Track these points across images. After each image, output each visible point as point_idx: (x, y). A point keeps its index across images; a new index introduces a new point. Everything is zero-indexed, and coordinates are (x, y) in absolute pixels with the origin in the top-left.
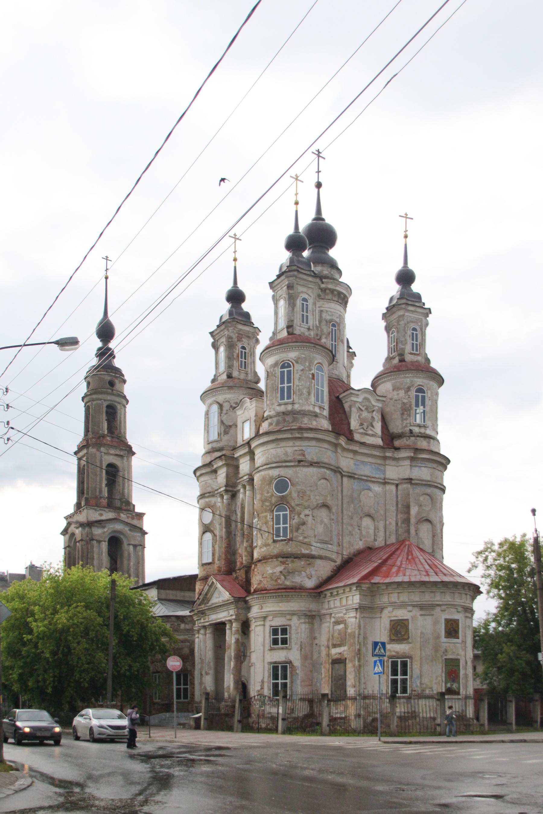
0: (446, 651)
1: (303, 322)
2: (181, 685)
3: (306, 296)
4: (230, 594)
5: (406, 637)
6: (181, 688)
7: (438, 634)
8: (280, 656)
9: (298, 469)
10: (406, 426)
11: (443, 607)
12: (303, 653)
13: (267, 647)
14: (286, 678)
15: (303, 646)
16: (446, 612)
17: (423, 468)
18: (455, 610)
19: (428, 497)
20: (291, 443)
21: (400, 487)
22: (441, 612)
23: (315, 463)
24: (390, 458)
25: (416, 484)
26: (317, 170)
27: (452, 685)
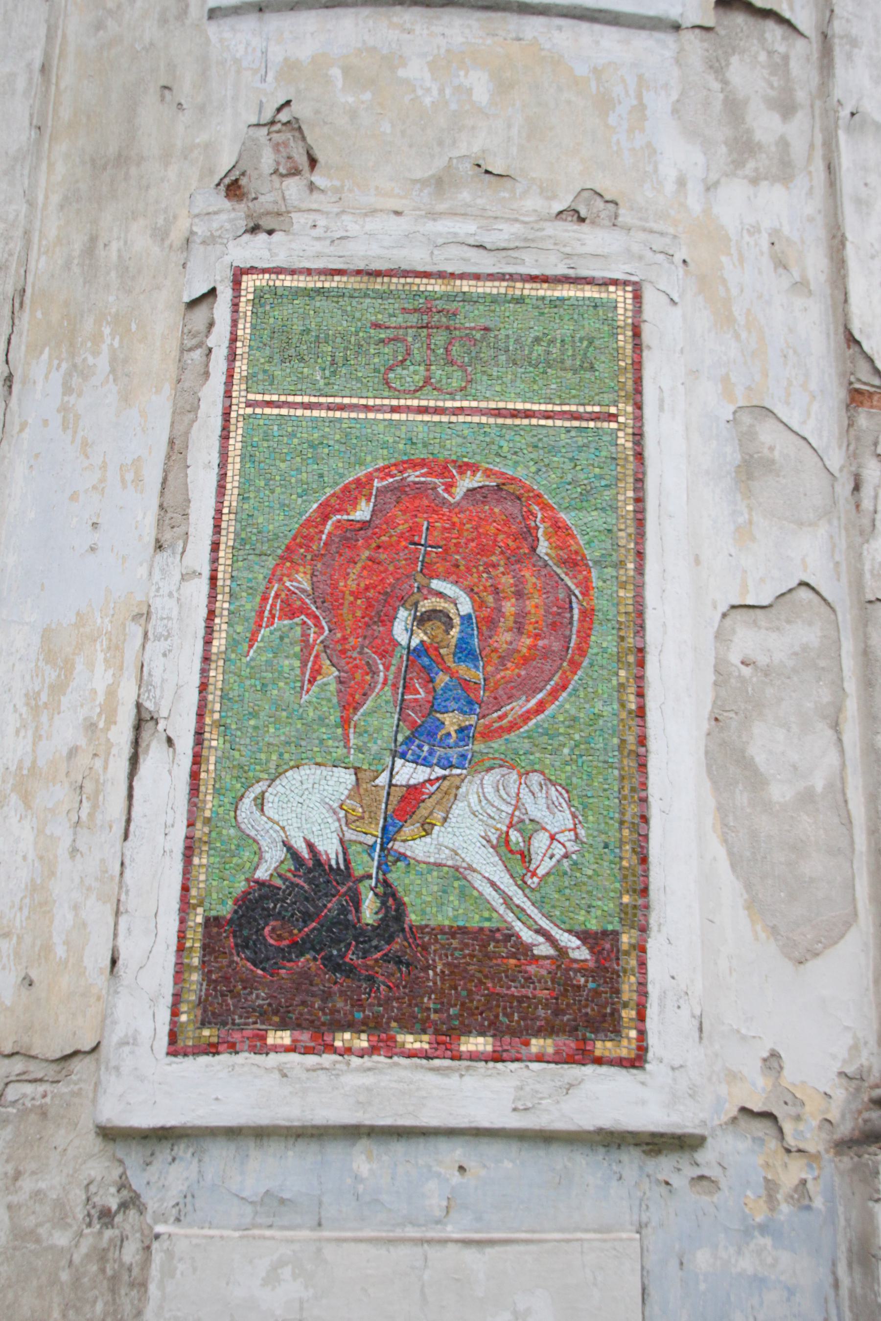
0: (293, 140)
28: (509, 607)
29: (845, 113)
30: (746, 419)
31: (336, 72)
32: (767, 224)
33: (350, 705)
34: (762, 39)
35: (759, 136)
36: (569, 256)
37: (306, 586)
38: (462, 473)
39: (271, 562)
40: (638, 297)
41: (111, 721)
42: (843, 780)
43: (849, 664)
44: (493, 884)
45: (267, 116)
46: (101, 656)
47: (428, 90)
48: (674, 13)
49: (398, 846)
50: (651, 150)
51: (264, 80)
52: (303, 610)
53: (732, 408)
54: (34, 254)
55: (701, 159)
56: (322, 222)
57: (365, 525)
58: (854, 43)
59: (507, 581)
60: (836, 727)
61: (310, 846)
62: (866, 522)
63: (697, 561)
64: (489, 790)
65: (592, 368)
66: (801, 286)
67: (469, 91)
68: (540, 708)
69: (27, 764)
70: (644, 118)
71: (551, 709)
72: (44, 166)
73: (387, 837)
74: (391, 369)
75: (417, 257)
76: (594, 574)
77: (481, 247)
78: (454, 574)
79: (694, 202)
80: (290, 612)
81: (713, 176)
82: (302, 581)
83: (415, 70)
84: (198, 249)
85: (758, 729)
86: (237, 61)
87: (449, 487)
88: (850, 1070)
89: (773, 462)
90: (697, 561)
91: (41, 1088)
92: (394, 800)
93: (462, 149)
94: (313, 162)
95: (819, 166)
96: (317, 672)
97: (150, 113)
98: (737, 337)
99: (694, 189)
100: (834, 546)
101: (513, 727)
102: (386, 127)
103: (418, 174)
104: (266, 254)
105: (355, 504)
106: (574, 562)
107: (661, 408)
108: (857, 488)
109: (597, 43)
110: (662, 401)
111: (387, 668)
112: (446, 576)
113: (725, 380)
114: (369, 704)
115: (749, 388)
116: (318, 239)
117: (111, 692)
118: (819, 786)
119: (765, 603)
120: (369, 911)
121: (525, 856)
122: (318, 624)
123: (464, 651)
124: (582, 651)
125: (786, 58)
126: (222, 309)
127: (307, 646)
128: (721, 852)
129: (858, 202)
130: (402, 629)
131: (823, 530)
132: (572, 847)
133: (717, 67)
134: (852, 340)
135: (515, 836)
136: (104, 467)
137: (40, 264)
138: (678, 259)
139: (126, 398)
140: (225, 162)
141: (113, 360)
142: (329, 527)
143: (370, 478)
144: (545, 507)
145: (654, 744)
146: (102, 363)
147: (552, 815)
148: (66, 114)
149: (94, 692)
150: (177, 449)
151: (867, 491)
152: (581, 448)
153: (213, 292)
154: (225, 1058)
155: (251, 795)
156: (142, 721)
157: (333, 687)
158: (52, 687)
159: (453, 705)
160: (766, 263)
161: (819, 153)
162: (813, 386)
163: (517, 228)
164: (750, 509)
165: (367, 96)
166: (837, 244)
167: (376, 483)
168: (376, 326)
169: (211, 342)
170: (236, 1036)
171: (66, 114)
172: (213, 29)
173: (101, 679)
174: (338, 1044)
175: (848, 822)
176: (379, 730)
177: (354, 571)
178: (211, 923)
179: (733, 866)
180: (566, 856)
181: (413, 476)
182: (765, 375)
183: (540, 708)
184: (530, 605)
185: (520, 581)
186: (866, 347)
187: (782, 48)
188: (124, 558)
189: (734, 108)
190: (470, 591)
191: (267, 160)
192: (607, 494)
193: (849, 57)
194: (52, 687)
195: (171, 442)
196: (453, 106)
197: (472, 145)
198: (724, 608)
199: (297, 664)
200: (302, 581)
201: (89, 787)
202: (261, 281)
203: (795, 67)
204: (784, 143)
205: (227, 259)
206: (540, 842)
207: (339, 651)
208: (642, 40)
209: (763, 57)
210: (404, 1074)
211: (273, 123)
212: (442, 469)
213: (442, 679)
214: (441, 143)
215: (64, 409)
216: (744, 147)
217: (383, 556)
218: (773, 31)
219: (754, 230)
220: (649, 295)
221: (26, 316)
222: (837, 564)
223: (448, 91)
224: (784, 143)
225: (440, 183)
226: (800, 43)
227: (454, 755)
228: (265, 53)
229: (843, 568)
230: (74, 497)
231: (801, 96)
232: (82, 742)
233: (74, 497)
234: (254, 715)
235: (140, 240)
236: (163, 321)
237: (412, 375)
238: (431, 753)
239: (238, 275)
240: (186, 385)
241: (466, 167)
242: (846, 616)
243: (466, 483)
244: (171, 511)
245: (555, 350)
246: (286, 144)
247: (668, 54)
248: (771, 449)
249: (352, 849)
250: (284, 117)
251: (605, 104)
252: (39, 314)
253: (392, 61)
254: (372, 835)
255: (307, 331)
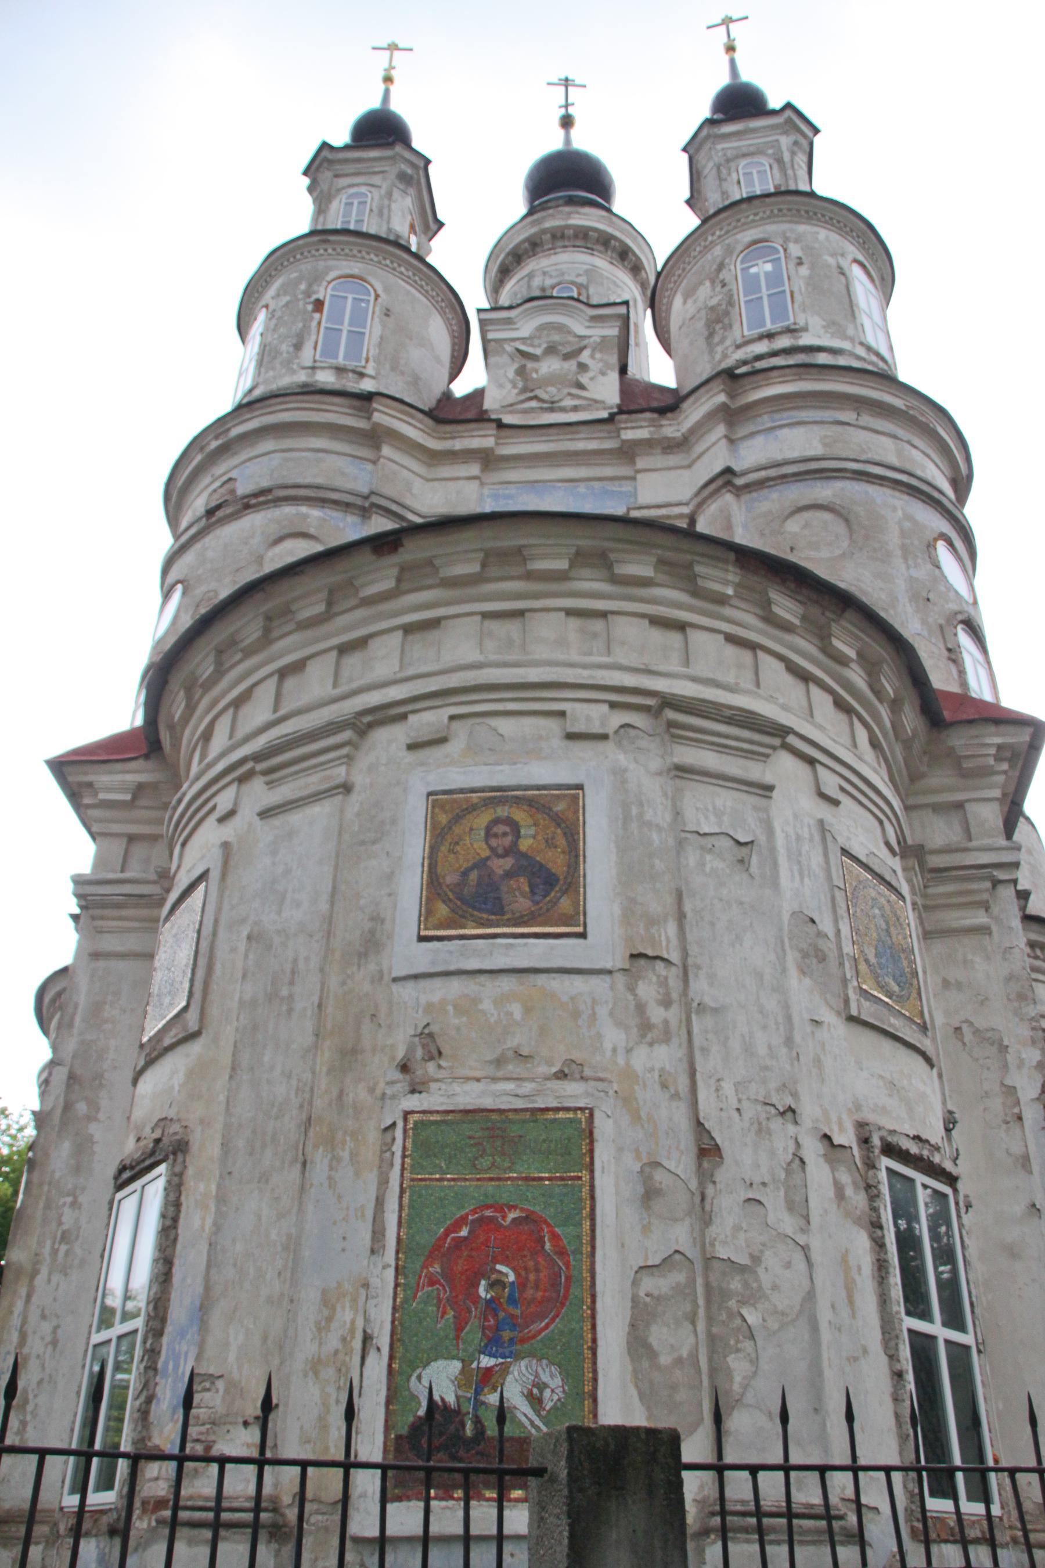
0: (430, 1045)
4: (40, 1118)
7: (377, 919)
10: (725, 356)
11: (427, 721)
16: (455, 747)
17: (785, 431)
18: (552, 725)
19: (827, 516)
22: (410, 757)
23: (256, 495)
24: (648, 445)
25: (761, 484)
26: (563, 103)
28: (532, 1277)
29: (695, 1005)
30: (647, 1169)
31: (450, 1008)
32: (657, 1066)
33: (459, 1329)
34: (654, 970)
35: (654, 1020)
36: (558, 1097)
37: (439, 1270)
38: (510, 1210)
39: (423, 1258)
40: (591, 1115)
41: (353, 1337)
42: (697, 1350)
43: (700, 1290)
44: (525, 1415)
45: (419, 1030)
46: (348, 1305)
47: (492, 1015)
48: (609, 965)
49: (482, 1398)
50: (599, 1036)
51: (417, 1012)
52: (438, 1282)
53: (640, 1165)
54: (315, 1098)
55: (623, 1036)
56: (443, 1087)
57: (465, 1238)
58: (699, 967)
59: (531, 1264)
60: (693, 1323)
61: (443, 1399)
62: (707, 1217)
63: (623, 1246)
64: (523, 1368)
65: (570, 1154)
66: (676, 1096)
67: (512, 1014)
68: (547, 1326)
69: (316, 1357)
70: (595, 1019)
71: (552, 1326)
72: (319, 1053)
73: (477, 1393)
74: (476, 1159)
75: (488, 1103)
76: (571, 1258)
77: (517, 1096)
78: (506, 1262)
79: (621, 1060)
80: (432, 1283)
81: (630, 1045)
82: (436, 1268)
83: (486, 1005)
84: (388, 1101)
85: (654, 1328)
86: (405, 1003)
87: (504, 1217)
88: (698, 1498)
89: (661, 1189)
90: (623, 1246)
91: (325, 1517)
92: (480, 1375)
93: (509, 1045)
94: (440, 1053)
95: (684, 1031)
96: (444, 1313)
97: (366, 1027)
98: (643, 1126)
99: (621, 1052)
100: (693, 1230)
101: (534, 1337)
102: (474, 1035)
103: (489, 1058)
104: (418, 1104)
105: (460, 1229)
106: (562, 1253)
107: (603, 1172)
108: (703, 1199)
109: (572, 984)
110: (603, 1168)
111: (476, 1309)
112: (502, 1263)
113: (637, 1150)
114: (468, 1328)
115: (648, 1153)
116: (442, 1095)
117: (353, 1322)
118: (685, 1355)
119: (657, 1263)
120: (469, 1430)
121: (540, 1401)
122: (446, 1291)
123: (512, 1300)
124: (566, 1297)
125: (666, 978)
126: (399, 1133)
127: (439, 1300)
128: (634, 1392)
129: (703, 1049)
130: (483, 1291)
131: (687, 1222)
132: (562, 1395)
133: (632, 989)
134: (699, 1124)
135: (535, 1391)
136: (348, 1208)
137: (318, 1103)
138: (611, 1093)
139: (357, 1174)
140: (400, 1054)
141: (351, 1153)
142: (449, 1240)
143: (467, 1215)
144: (549, 1225)
145: (601, 1342)
146: (346, 1155)
147: (554, 1381)
148: (329, 1026)
149: (345, 1322)
150: (380, 1202)
151: (708, 1201)
152: (565, 1195)
153: (394, 1124)
154: (405, 1504)
155: (415, 1375)
156: (367, 1338)
157: (451, 1320)
158: (327, 1319)
159: (507, 1327)
160: (657, 1087)
161: (684, 1023)
162: (682, 1147)
163: (533, 1085)
164: (649, 1216)
165: (464, 1019)
166: (692, 1073)
167: (470, 1217)
168: (470, 1137)
169: (394, 1149)
170: (410, 1493)
171: (329, 1026)
172: (395, 988)
173: (348, 1316)
174: (456, 1495)
175: (699, 1371)
176: (473, 1340)
177: (460, 1262)
178: (399, 1437)
179: (641, 1399)
180: (559, 1400)
181: (488, 1213)
182: (657, 1144)
183: (547, 1326)
184: (542, 1275)
185: (537, 1263)
186: (706, 1126)
187: (664, 973)
188: (357, 1256)
189: (641, 1008)
190: (514, 1269)
191: (419, 1053)
192: (577, 1218)
193: (696, 976)
194: (327, 1319)
195: (377, 1199)
196: (504, 1022)
197: (512, 1042)
198: (636, 1268)
199: (435, 1309)
200: (436, 1268)
201: (344, 1370)
202: (416, 1117)
203: (672, 982)
204: (666, 1022)
205: (401, 1107)
206: (547, 1393)
207: (453, 1302)
208: (595, 981)
209: (654, 979)
210: (485, 1510)
211: (421, 1034)
212: (500, 1208)
213: (502, 1315)
214: (499, 1041)
215: (330, 1178)
216: (645, 1027)
217: (474, 1254)
218: (659, 965)
219: (651, 1070)
220: (597, 1115)
221: (312, 1130)
222: (695, 1239)
223: (502, 1014)
224: (666, 1022)
225: (499, 1062)
226: (673, 969)
227: (507, 1351)
228: (417, 999)
229: (698, 1240)
230: (335, 1223)
231: (675, 996)
232: (340, 1347)
233: (335, 1223)
234: (416, 1335)
235: (363, 1094)
236: (373, 1136)
237: (485, 1162)
238: (497, 1351)
239: (406, 1114)
240: (384, 1169)
241: (510, 1053)
242: (699, 1267)
243: (512, 1215)
244: (378, 1233)
245: (553, 1146)
246: (427, 1045)
247: (606, 985)
248: (661, 1183)
249: (461, 1400)
250: (426, 1031)
251: (576, 1014)
252: (318, 1129)
253: (476, 1001)
254: (470, 1394)
255: (438, 1142)
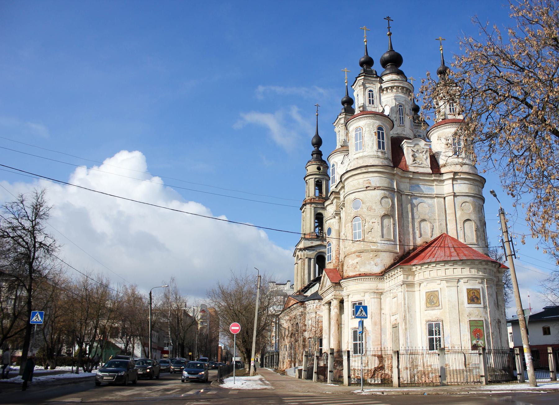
1: (370, 103)
2: (433, 335)
3: (372, 89)
5: (437, 304)
6: (433, 338)
8: (434, 314)
9: (367, 192)
12: (373, 320)
13: (350, 317)
14: (439, 335)
15: (373, 315)
20: (361, 176)
21: (446, 198)
27: (478, 342)
